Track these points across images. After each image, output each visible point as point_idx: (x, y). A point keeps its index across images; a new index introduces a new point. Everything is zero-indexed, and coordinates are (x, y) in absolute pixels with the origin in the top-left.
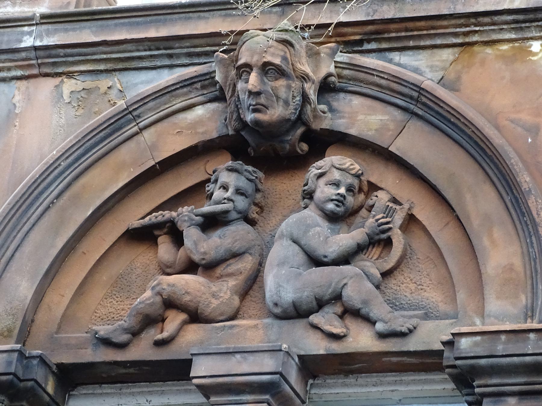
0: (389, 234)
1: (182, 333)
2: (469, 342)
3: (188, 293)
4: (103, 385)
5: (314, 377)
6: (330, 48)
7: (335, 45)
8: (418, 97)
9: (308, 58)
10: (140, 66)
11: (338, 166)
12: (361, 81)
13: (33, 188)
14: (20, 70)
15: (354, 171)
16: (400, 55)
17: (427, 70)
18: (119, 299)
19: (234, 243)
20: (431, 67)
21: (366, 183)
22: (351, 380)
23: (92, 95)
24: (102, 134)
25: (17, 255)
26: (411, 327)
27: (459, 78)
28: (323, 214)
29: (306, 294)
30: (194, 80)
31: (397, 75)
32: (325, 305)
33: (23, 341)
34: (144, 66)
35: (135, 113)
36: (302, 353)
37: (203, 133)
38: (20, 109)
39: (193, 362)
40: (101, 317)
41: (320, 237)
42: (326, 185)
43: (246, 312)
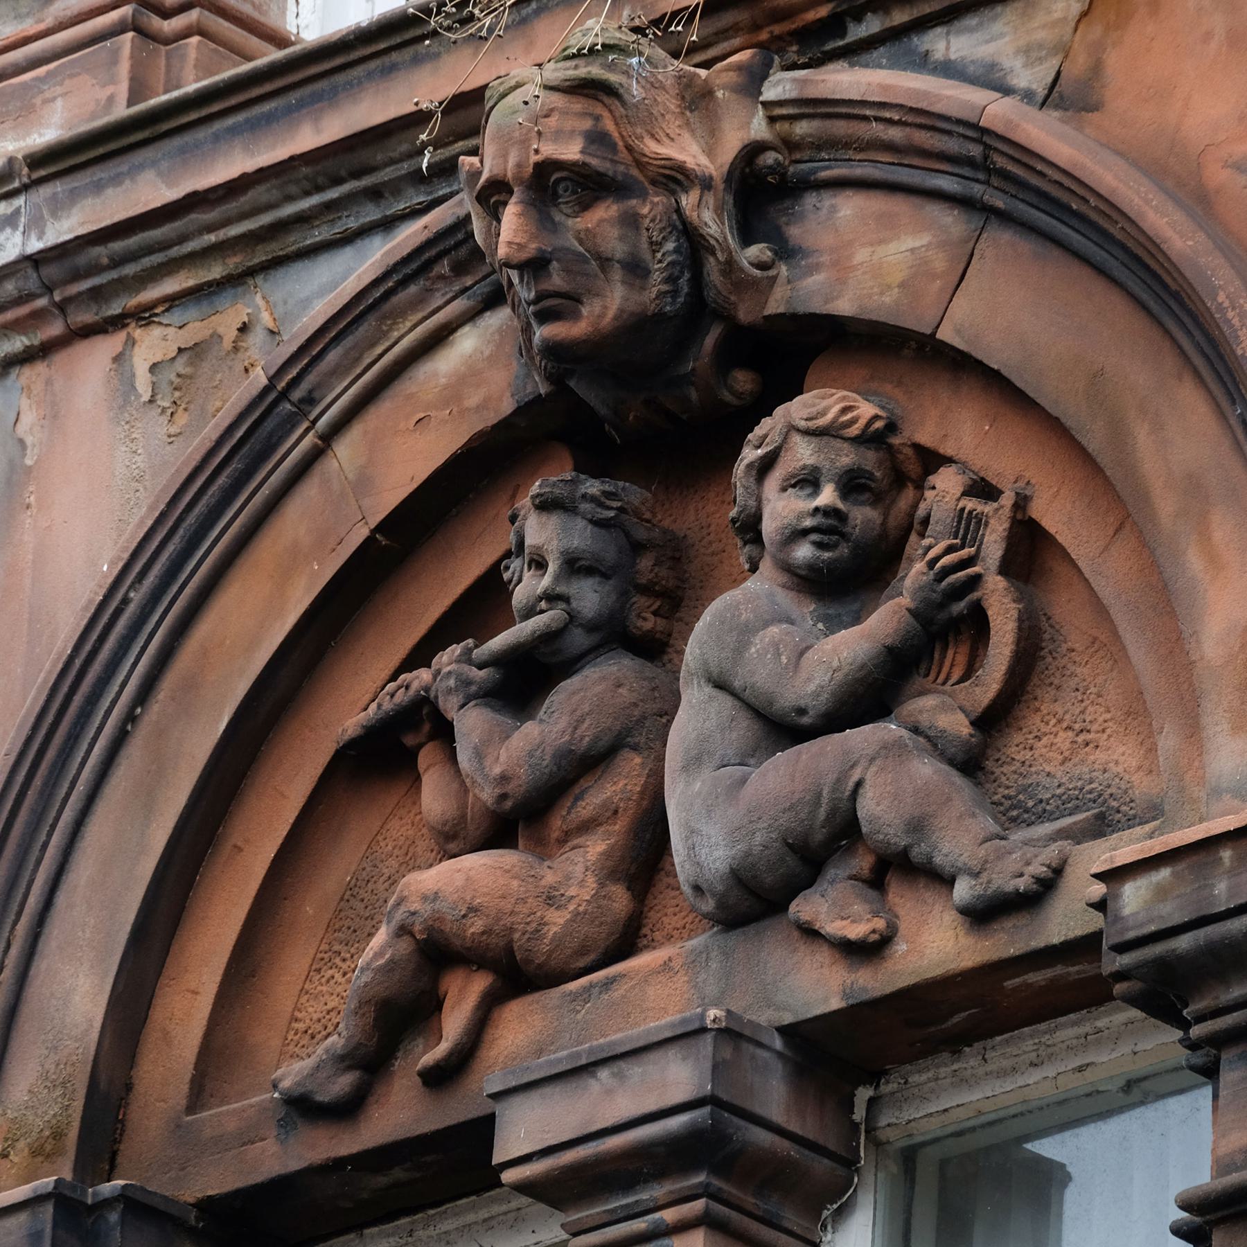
0: (974, 596)
1: (491, 1033)
2: (1143, 891)
3: (473, 910)
4: (367, 1231)
5: (875, 1076)
6: (739, 68)
7: (753, 56)
8: (986, 157)
9: (688, 113)
10: (308, 242)
11: (802, 424)
12: (847, 145)
13: (65, 689)
14: (19, 333)
15: (857, 426)
16: (948, 33)
17: (1017, 63)
18: (348, 963)
19: (576, 728)
20: (1026, 51)
21: (909, 451)
22: (970, 1061)
23: (204, 364)
24: (222, 480)
25: (61, 899)
26: (1042, 871)
27: (1097, 68)
28: (796, 580)
29: (758, 838)
30: (427, 255)
31: (919, 106)
32: (830, 856)
33: (107, 1156)
34: (318, 239)
35: (297, 395)
36: (788, 1019)
37: (479, 408)
38: (36, 451)
39: (497, 1120)
40: (310, 1032)
41: (779, 655)
42: (784, 489)
43: (658, 926)
